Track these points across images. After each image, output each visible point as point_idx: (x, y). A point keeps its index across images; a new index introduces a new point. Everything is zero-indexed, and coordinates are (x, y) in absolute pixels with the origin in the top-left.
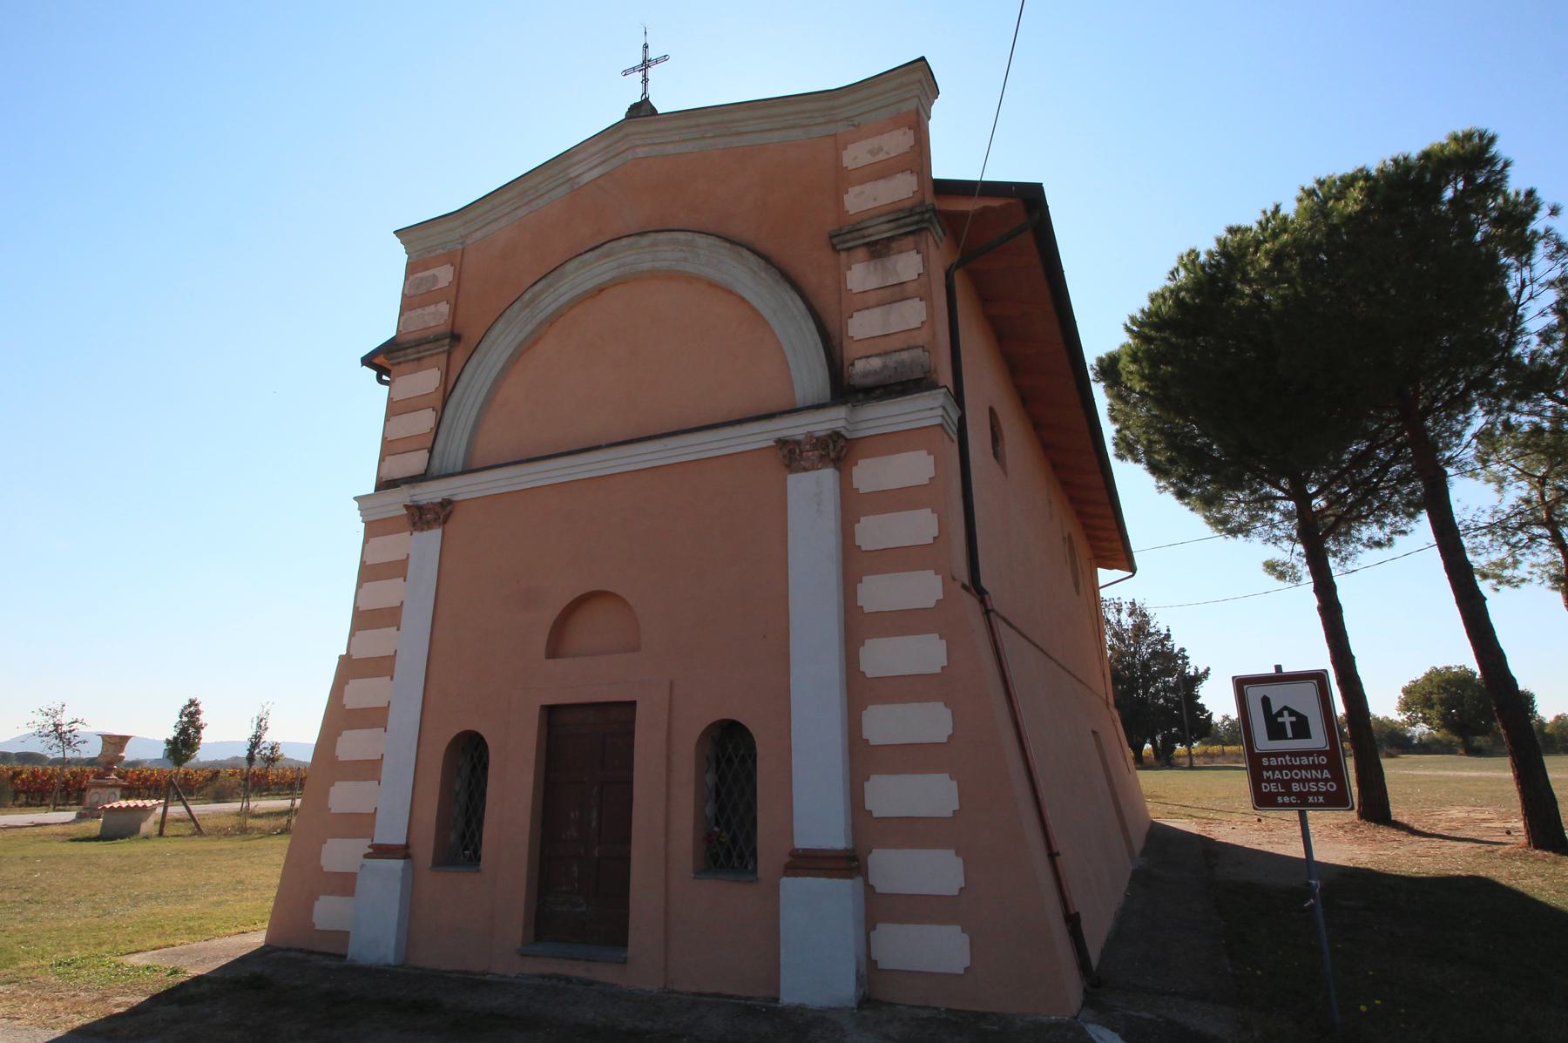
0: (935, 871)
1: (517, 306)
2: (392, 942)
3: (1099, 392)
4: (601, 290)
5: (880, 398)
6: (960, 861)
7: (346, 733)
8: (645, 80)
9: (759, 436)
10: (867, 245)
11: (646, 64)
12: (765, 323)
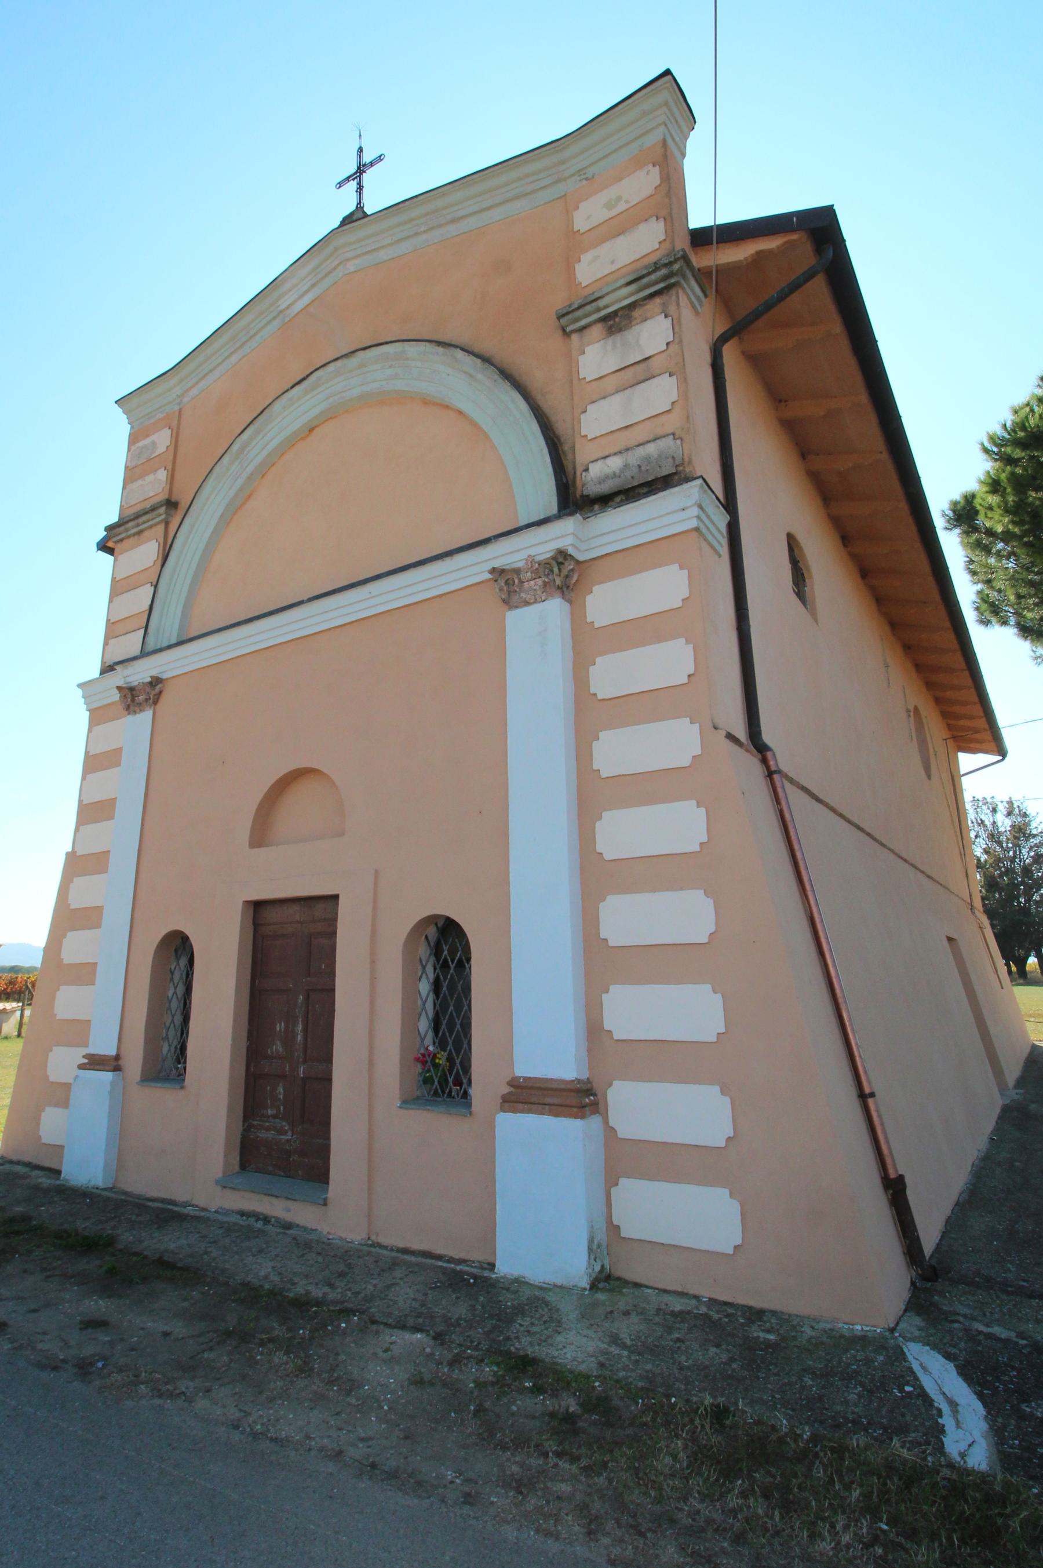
0: (694, 1114)
1: (226, 459)
3: (952, 546)
4: (311, 430)
6: (727, 1100)
7: (70, 934)
8: (360, 188)
9: (474, 568)
10: (604, 319)
11: (361, 169)
12: (487, 436)
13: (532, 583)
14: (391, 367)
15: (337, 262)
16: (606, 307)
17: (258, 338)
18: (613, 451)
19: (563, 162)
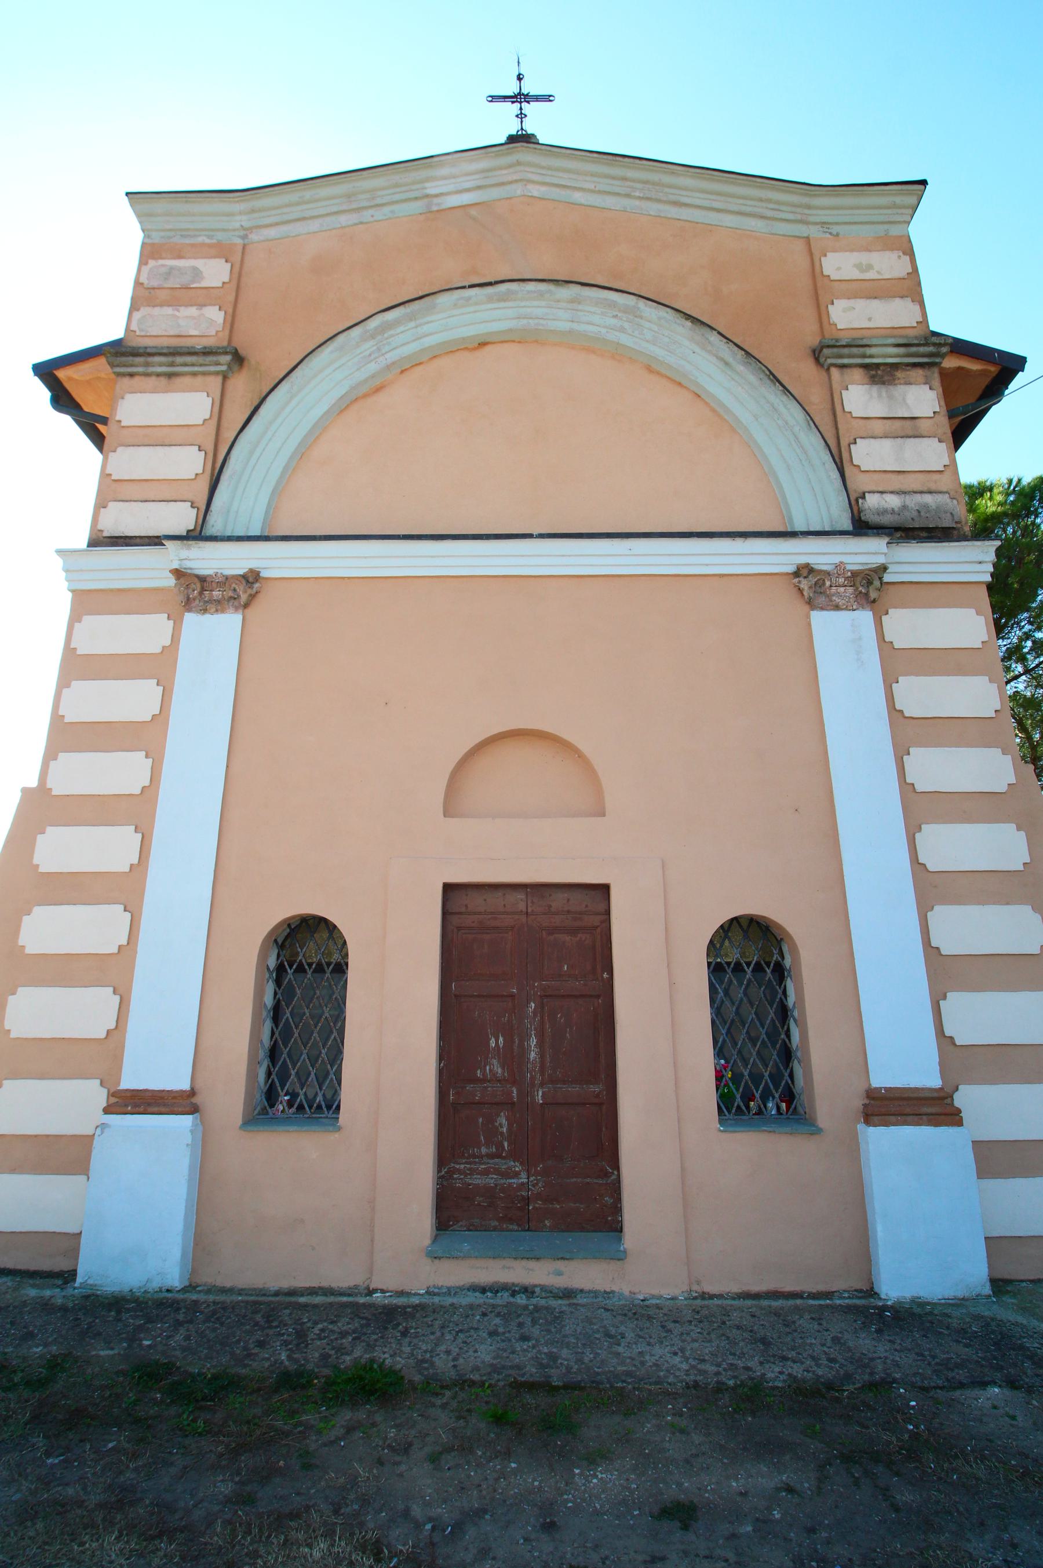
1: (356, 332)
2: (176, 1253)
4: (483, 344)
5: (940, 540)
9: (780, 557)
10: (866, 367)
13: (842, 589)
14: (615, 316)
15: (515, 177)
16: (871, 356)
17: (386, 210)
18: (891, 489)
19: (809, 207)
